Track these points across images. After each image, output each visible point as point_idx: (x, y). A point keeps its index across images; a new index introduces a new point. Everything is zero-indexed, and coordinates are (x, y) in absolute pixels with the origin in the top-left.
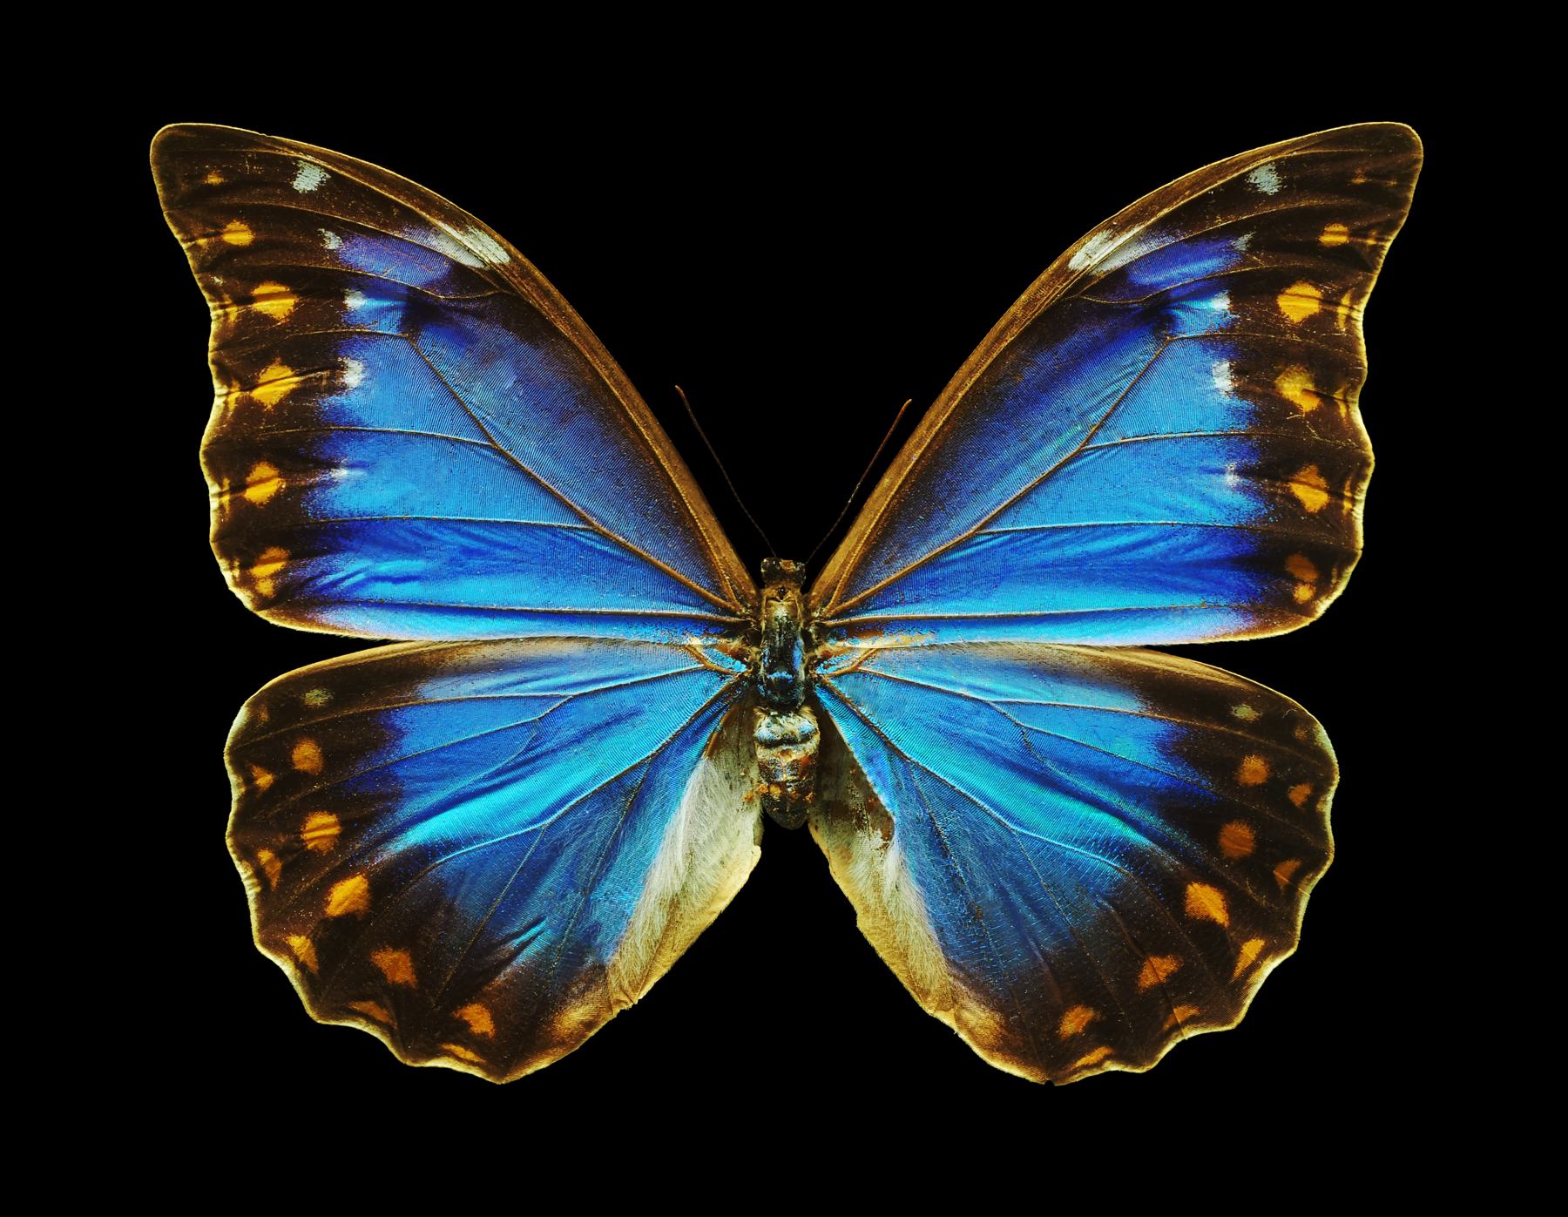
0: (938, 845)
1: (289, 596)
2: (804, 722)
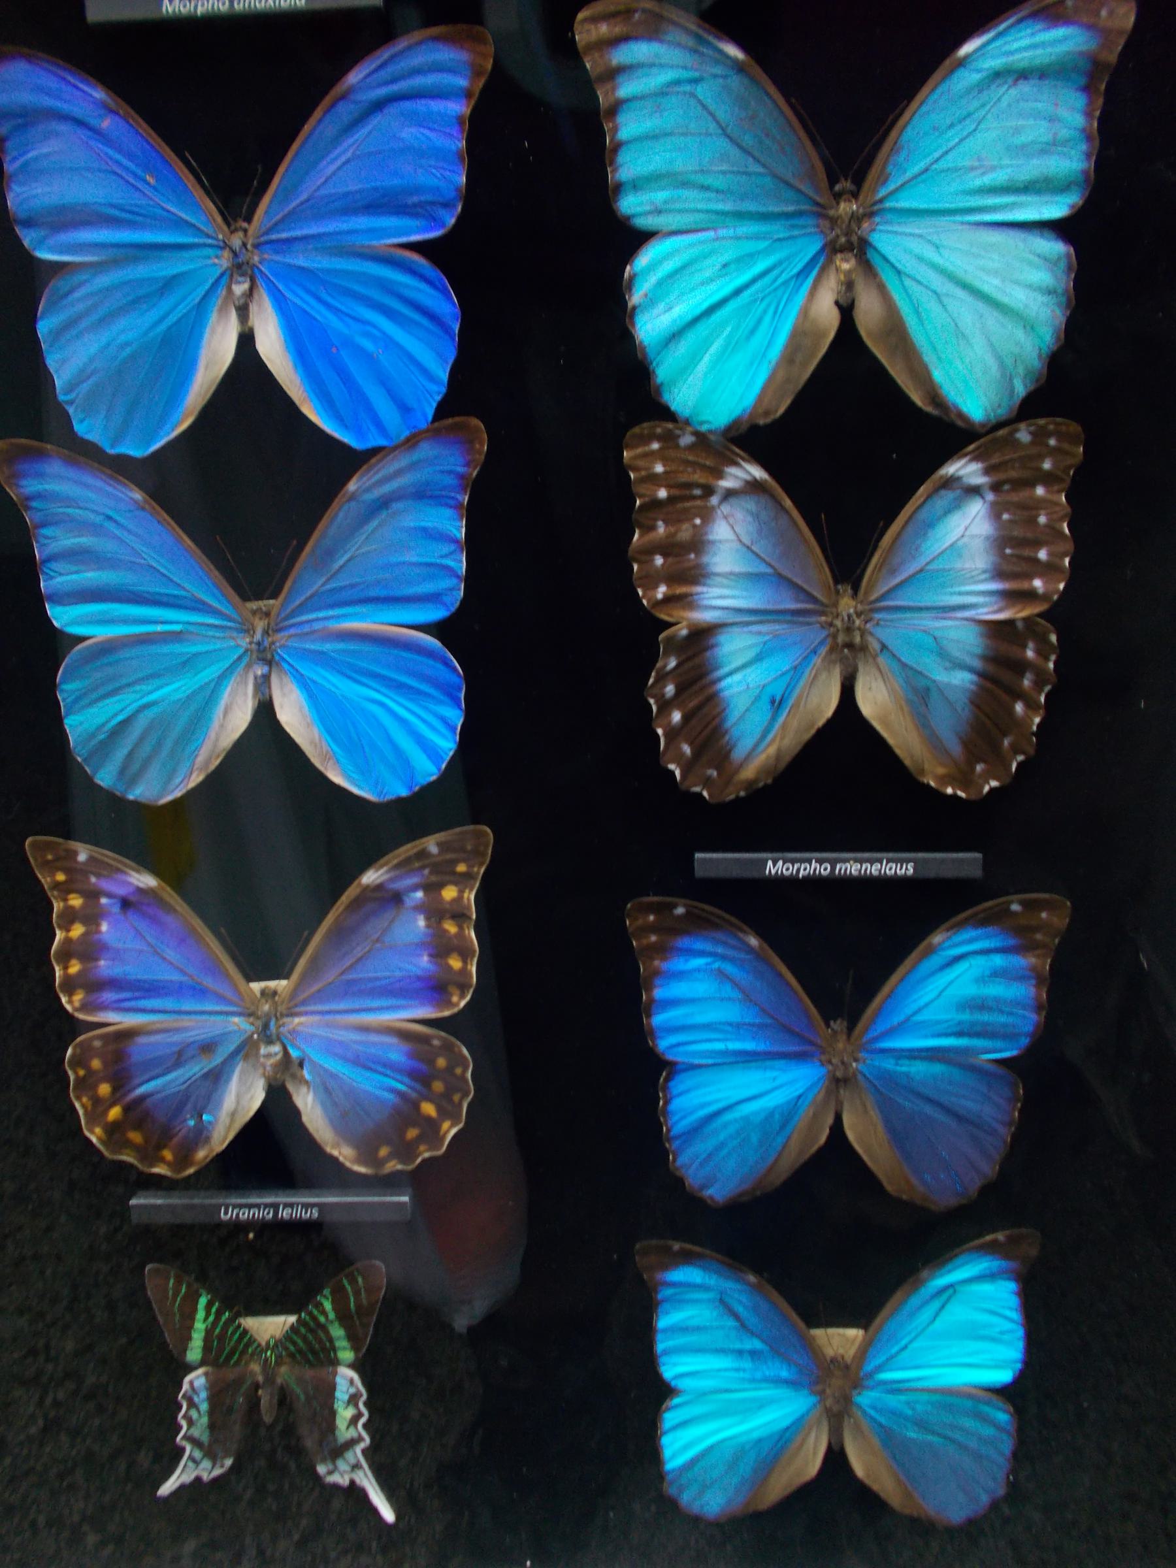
0: (327, 1091)
1: (84, 1007)
2: (276, 1048)
